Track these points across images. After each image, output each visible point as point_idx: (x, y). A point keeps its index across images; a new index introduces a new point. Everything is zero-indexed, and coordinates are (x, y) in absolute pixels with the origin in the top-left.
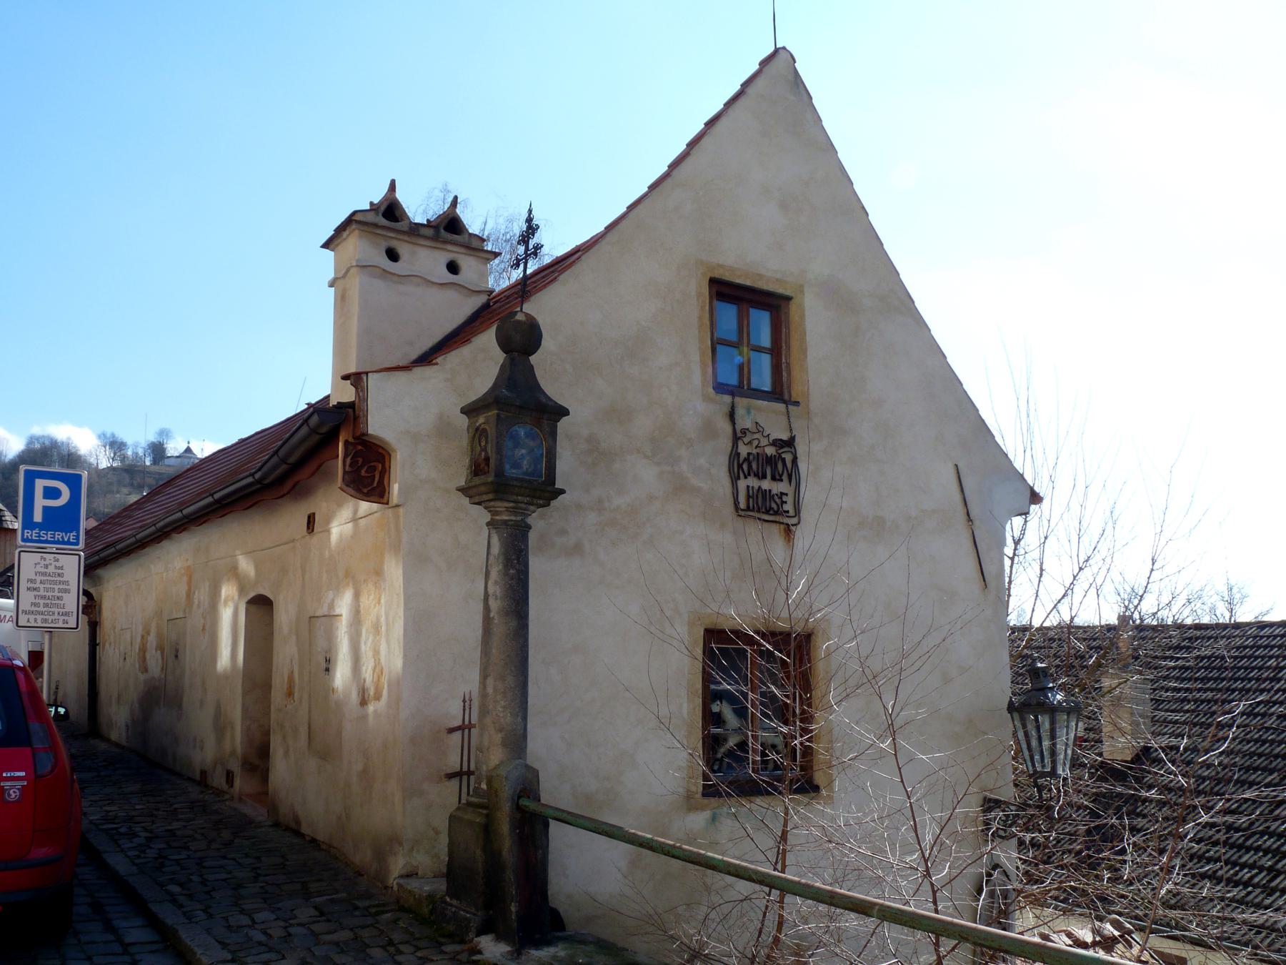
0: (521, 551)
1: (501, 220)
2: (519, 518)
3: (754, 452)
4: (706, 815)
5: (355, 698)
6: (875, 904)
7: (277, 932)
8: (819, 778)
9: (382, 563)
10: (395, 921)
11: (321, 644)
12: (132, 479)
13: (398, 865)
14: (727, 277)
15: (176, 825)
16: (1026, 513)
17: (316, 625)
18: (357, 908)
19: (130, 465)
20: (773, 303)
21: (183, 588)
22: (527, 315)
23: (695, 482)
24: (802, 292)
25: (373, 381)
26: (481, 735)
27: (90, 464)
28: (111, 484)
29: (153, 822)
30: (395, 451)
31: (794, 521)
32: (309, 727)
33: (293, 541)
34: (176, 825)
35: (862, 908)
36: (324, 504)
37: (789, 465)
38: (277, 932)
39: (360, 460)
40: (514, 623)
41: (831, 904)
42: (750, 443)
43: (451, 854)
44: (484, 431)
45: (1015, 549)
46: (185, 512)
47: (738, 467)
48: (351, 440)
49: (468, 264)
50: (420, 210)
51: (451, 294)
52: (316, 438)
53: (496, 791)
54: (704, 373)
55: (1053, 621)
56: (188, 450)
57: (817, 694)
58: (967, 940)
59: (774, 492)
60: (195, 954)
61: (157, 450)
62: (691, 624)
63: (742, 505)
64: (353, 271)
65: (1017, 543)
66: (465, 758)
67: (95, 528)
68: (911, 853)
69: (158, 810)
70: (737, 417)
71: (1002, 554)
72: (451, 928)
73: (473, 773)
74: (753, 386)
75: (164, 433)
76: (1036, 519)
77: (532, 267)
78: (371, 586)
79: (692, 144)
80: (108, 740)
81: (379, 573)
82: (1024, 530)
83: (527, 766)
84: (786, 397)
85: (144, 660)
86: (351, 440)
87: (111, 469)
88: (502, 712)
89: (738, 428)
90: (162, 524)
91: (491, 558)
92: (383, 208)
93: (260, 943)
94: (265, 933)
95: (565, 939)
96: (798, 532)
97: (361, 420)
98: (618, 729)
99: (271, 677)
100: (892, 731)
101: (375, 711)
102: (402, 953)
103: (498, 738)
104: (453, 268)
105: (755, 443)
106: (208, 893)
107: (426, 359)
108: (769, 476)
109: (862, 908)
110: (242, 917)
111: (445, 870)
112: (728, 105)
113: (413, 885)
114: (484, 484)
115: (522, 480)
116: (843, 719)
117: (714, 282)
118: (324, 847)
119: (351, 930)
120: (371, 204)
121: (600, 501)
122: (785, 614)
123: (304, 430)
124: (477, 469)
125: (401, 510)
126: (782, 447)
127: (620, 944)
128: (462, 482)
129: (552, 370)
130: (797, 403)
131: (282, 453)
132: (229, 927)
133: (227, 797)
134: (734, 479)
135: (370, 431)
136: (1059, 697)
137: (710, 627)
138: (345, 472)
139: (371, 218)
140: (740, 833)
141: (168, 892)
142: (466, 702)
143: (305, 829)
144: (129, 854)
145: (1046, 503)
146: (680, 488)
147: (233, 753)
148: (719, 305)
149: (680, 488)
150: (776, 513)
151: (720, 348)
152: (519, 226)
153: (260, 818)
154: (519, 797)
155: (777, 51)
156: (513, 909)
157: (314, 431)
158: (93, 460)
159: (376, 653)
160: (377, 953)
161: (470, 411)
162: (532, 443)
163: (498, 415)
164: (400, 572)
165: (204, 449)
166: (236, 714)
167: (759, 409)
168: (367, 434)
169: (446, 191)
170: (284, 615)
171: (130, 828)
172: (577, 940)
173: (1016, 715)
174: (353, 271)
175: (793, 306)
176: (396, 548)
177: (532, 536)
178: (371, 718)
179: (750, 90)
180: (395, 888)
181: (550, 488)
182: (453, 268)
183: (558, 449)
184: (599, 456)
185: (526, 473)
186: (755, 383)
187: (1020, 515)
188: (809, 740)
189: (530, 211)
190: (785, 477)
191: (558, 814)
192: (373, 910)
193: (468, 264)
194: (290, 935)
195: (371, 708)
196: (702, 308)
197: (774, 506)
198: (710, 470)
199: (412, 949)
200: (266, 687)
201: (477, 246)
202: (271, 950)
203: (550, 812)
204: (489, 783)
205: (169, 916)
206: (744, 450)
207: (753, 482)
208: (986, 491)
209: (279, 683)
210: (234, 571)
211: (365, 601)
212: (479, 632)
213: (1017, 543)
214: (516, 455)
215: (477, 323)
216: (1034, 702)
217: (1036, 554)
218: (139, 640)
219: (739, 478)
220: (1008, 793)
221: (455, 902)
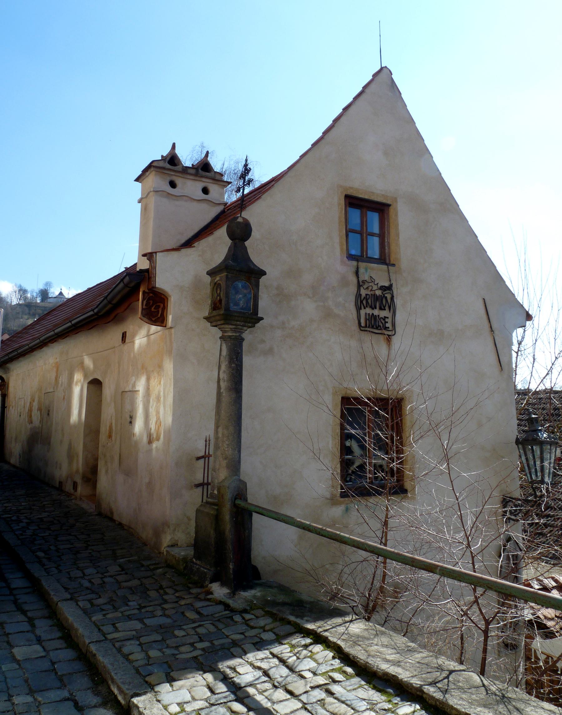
0: (238, 353)
1: (232, 162)
2: (238, 334)
3: (369, 293)
5: (145, 439)
6: (438, 566)
7: (97, 581)
8: (407, 485)
11: (128, 407)
12: (30, 310)
13: (166, 540)
14: (355, 194)
15: (44, 515)
16: (525, 326)
17: (125, 395)
18: (143, 566)
19: (29, 303)
20: (382, 208)
21: (54, 375)
22: (244, 218)
23: (336, 311)
24: (396, 201)
25: (159, 257)
26: (215, 462)
27: (7, 302)
28: (18, 313)
29: (31, 513)
30: (170, 296)
33: (114, 347)
34: (44, 515)
35: (430, 568)
36: (131, 327)
37: (389, 301)
38: (97, 581)
39: (151, 302)
40: (234, 396)
41: (413, 566)
42: (367, 288)
43: (196, 532)
44: (219, 284)
45: (519, 347)
46: (56, 331)
47: (361, 302)
48: (147, 291)
49: (214, 188)
50: (189, 158)
51: (204, 206)
52: (127, 289)
53: (222, 496)
54: (342, 249)
55: (542, 387)
56: (61, 294)
57: (405, 435)
58: (491, 589)
59: (381, 316)
60: (50, 595)
61: (44, 294)
62: (335, 394)
63: (363, 324)
65: (520, 343)
66: (206, 475)
67: (8, 339)
68: (459, 532)
69: (34, 505)
70: (360, 274)
71: (511, 349)
72: (196, 578)
74: (369, 256)
75: (48, 284)
76: (531, 329)
77: (247, 191)
78: (156, 374)
79: (336, 121)
80: (9, 463)
81: (160, 367)
82: (523, 338)
83: (240, 480)
84: (387, 261)
85: (31, 416)
86: (147, 291)
87: (18, 305)
89: (361, 280)
90: (43, 338)
91: (222, 357)
92: (168, 159)
93: (87, 588)
94: (90, 582)
95: (261, 585)
97: (153, 279)
98: (293, 460)
100: (447, 459)
101: (156, 447)
103: (224, 463)
104: (205, 191)
105: (370, 288)
106: (59, 557)
107: (188, 244)
108: (378, 307)
109: (430, 568)
110: (78, 571)
111: (193, 542)
112: (356, 98)
113: (175, 551)
115: (240, 313)
116: (420, 450)
117: (347, 197)
118: (126, 528)
119: (139, 579)
120: (162, 156)
121: (283, 323)
122: (385, 388)
123: (121, 285)
124: (215, 306)
125: (173, 330)
126: (385, 290)
127: (292, 589)
128: (206, 314)
129: (257, 251)
130: (394, 265)
131: (109, 298)
132: (70, 578)
133: (73, 497)
134: (358, 309)
136: (545, 435)
138: (143, 309)
139: (161, 164)
140: (361, 521)
141: (37, 557)
142: (207, 442)
143: (116, 517)
144: (17, 533)
145: (536, 320)
146: (328, 315)
147: (77, 471)
148: (350, 210)
149: (328, 315)
151: (351, 234)
152: (241, 168)
153: (92, 510)
154: (235, 499)
155: (382, 68)
156: (231, 567)
157: (126, 285)
158: (9, 300)
159: (158, 413)
160: (153, 594)
161: (212, 273)
162: (245, 291)
163: (227, 275)
164: (172, 366)
165: (69, 294)
166: (80, 448)
167: (373, 269)
168: (155, 287)
169: (203, 147)
170: (108, 391)
171: (18, 517)
172: (267, 585)
173: (520, 446)
174: (151, 194)
175: (391, 210)
176: (170, 352)
177: (245, 344)
178: (154, 452)
179: (367, 91)
181: (254, 317)
182: (205, 191)
183: (260, 293)
184: (283, 297)
185: (242, 309)
186: (370, 254)
187: (521, 327)
188: (401, 463)
189: (246, 160)
190: (387, 308)
191: (257, 509)
192: (152, 567)
193: (214, 188)
194: (104, 582)
195: (154, 445)
200: (97, 432)
201: (219, 179)
202: (93, 592)
203: (252, 508)
204: (219, 491)
205: (37, 571)
206: (363, 292)
207: (369, 311)
208: (500, 312)
209: (104, 430)
210: (82, 364)
211: (154, 383)
212: (214, 401)
213: (520, 343)
214: (236, 298)
215: (218, 222)
216: (530, 438)
217: (531, 350)
218: (28, 404)
219: (361, 309)
220: (517, 493)
221: (198, 562)
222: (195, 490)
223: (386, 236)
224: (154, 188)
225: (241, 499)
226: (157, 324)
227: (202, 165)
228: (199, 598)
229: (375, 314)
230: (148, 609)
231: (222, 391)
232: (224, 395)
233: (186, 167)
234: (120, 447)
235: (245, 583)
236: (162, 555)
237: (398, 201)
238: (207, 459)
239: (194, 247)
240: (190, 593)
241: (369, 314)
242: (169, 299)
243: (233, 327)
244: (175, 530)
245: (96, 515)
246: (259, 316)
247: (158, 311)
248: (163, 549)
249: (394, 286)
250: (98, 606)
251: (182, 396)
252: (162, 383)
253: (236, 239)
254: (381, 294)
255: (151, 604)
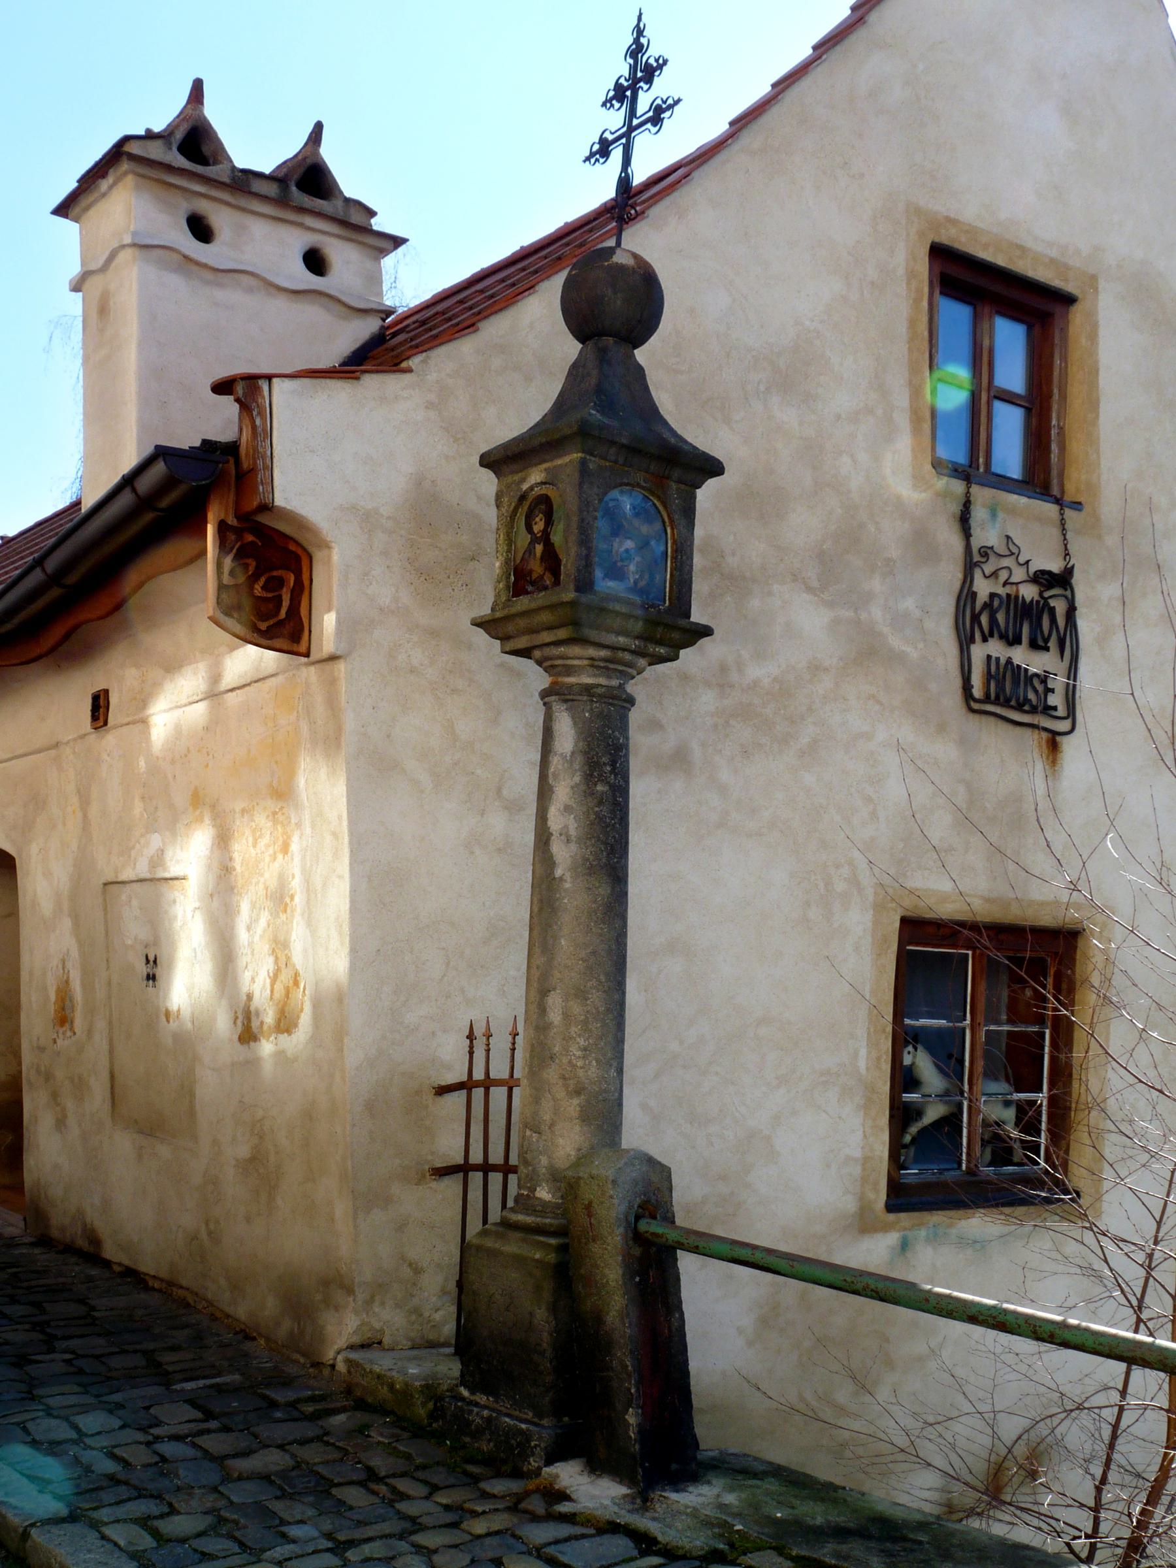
2: (615, 682)
3: (1002, 591)
4: (892, 1239)
5: (224, 1025)
9: (291, 774)
10: (362, 1430)
11: (133, 930)
13: (340, 1331)
18: (273, 1404)
23: (895, 642)
25: (283, 398)
30: (326, 545)
31: (1063, 726)
32: (112, 1077)
33: (57, 745)
37: (1061, 621)
40: (604, 890)
42: (995, 574)
44: (545, 500)
47: (973, 619)
48: (232, 521)
49: (343, 256)
51: (312, 312)
62: (879, 908)
63: (977, 692)
64: (125, 256)
72: (486, 1446)
73: (514, 1170)
78: (261, 819)
81: (282, 793)
84: (1055, 491)
86: (232, 521)
88: (575, 1053)
89: (976, 544)
91: (555, 763)
92: (179, 135)
93: (113, 1480)
96: (1066, 743)
98: (760, 1087)
99: (17, 992)
101: (280, 1055)
102: (403, 1497)
103: (572, 1106)
104: (315, 261)
105: (1003, 575)
110: (54, 1422)
113: (381, 1363)
114: (552, 607)
117: (940, 253)
119: (281, 1447)
121: (723, 669)
125: (341, 667)
126: (1050, 587)
128: (484, 610)
130: (1077, 506)
131: (51, 564)
134: (965, 642)
135: (279, 501)
137: (909, 914)
138: (221, 587)
139: (155, 151)
143: (110, 1252)
146: (868, 652)
149: (868, 652)
150: (1034, 710)
154: (638, 1218)
160: (354, 1496)
162: (645, 529)
163: (583, 463)
164: (340, 789)
167: (1013, 511)
168: (267, 507)
174: (125, 256)
175: (1077, 315)
176: (330, 742)
177: (635, 717)
180: (341, 1367)
189: (639, 31)
190: (1053, 643)
191: (692, 1241)
192: (309, 1409)
193: (343, 256)
194: (164, 1459)
195: (266, 1047)
196: (917, 301)
197: (1031, 696)
198: (919, 617)
199: (422, 1490)
206: (983, 588)
207: (996, 648)
211: (241, 849)
221: (482, 1399)
222: (434, 1185)
223: (1055, 407)
224: (134, 234)
225: (654, 1217)
226: (278, 643)
227: (301, 170)
228: (526, 1512)
229: (1016, 661)
230: (367, 1550)
231: (558, 872)
232: (567, 885)
233: (245, 172)
234: (111, 1051)
235: (674, 1466)
236: (326, 1372)
237: (1100, 288)
238: (478, 1093)
239: (409, 370)
240: (486, 1496)
241: (998, 659)
242: (318, 556)
243: (603, 653)
244: (370, 1302)
245: (33, 1245)
246: (692, 619)
247: (279, 600)
248: (331, 1354)
249: (1077, 580)
250: (183, 1541)
251: (380, 889)
252: (294, 847)
253: (601, 334)
254: (1037, 598)
255: (370, 1532)
